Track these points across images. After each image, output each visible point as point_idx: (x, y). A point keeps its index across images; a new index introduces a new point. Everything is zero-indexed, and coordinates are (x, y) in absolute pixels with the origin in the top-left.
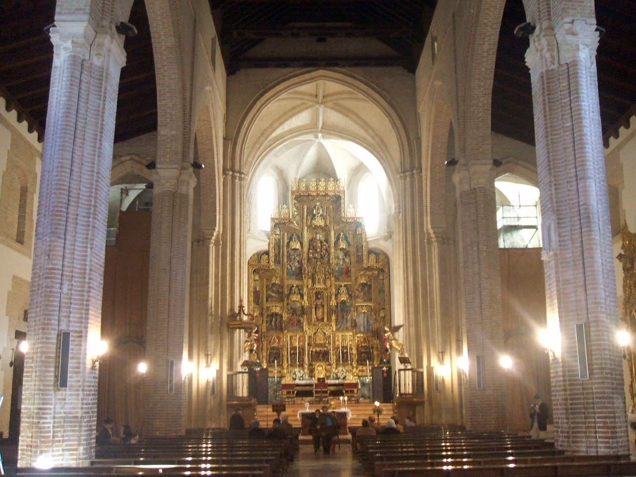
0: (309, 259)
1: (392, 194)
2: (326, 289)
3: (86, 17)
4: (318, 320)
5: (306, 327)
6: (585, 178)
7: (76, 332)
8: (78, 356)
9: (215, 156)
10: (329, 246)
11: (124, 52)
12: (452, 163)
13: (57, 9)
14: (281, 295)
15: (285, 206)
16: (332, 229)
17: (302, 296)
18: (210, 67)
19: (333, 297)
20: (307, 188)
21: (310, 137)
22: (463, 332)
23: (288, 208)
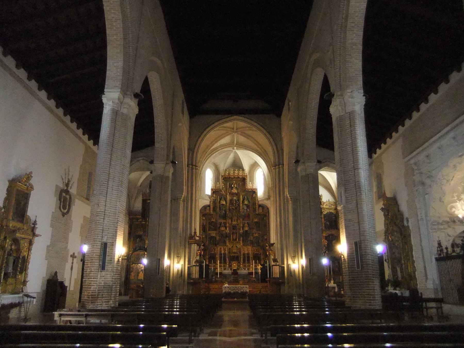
0: (229, 209)
1: (270, 177)
2: (238, 224)
3: (119, 90)
4: (233, 240)
5: (228, 244)
6: (358, 169)
7: (110, 243)
8: (111, 255)
9: (184, 158)
10: (240, 203)
11: (138, 107)
12: (297, 162)
13: (106, 86)
14: (215, 227)
15: (218, 183)
16: (241, 194)
17: (226, 228)
18: (181, 115)
19: (241, 229)
20: (229, 174)
21: (230, 149)
22: (303, 246)
23: (220, 184)
